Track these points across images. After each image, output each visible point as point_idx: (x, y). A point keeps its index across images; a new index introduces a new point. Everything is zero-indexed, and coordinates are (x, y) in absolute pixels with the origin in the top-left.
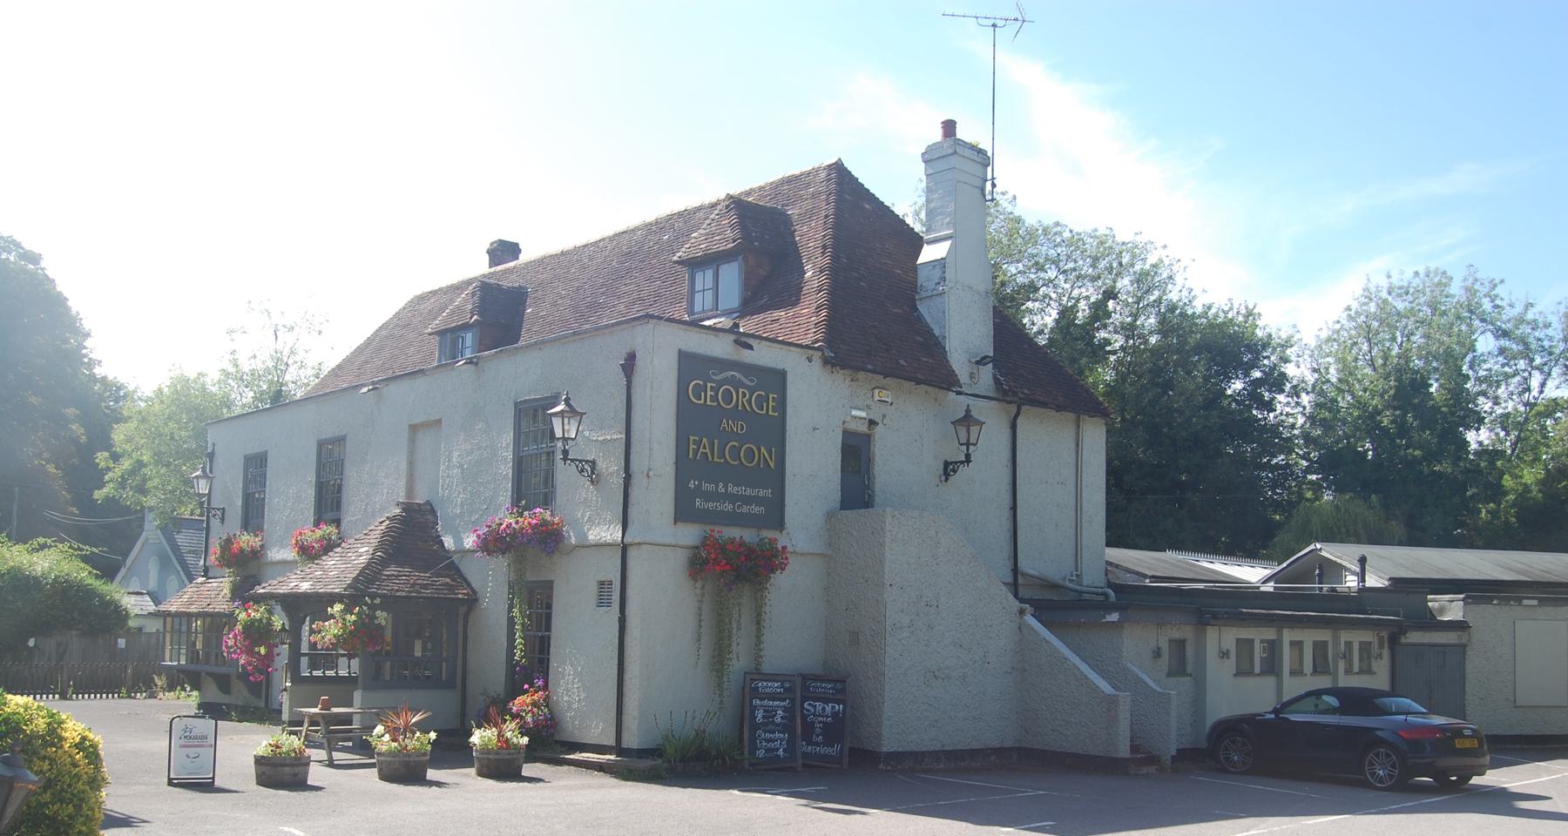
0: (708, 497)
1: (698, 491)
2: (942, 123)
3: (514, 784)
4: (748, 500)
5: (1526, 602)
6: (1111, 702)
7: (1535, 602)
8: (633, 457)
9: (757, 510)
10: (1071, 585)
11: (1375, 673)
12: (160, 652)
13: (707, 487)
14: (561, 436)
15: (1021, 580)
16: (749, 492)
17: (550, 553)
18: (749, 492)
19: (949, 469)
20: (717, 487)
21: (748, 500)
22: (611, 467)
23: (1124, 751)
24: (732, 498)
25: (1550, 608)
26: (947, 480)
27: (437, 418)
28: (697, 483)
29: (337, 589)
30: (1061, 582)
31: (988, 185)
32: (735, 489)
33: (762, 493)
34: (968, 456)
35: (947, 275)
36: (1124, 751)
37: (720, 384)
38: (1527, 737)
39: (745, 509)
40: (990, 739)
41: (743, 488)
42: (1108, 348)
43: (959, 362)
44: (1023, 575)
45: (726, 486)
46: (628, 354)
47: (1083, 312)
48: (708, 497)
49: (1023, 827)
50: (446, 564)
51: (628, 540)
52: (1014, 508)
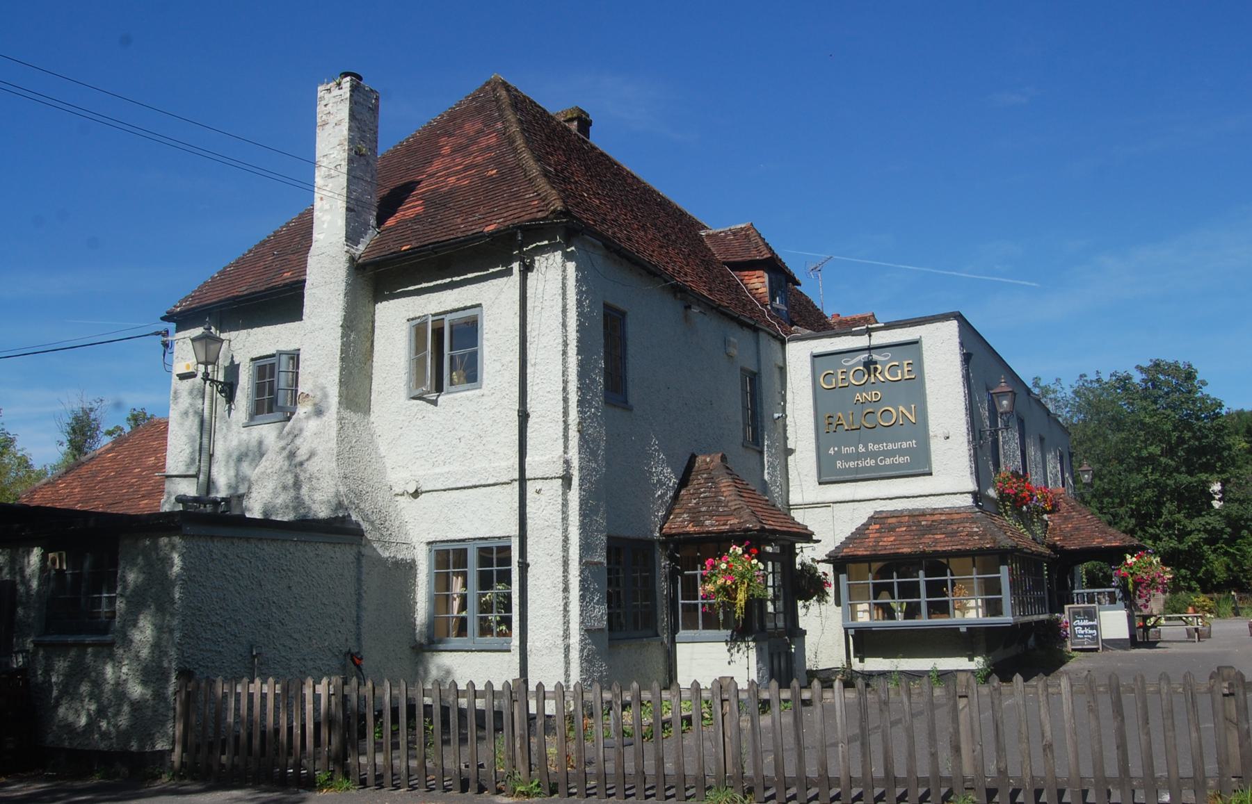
0: (848, 458)
1: (838, 455)
2: (302, 320)
4: (891, 454)
8: (847, 499)
12: (367, 392)
13: (844, 450)
14: (746, 694)
17: (469, 382)
18: (890, 446)
20: (857, 448)
21: (891, 454)
24: (874, 455)
27: (805, 676)
28: (836, 449)
31: (956, 516)
32: (876, 447)
33: (905, 445)
39: (888, 461)
41: (885, 444)
44: (189, 466)
45: (866, 446)
46: (349, 260)
48: (848, 458)
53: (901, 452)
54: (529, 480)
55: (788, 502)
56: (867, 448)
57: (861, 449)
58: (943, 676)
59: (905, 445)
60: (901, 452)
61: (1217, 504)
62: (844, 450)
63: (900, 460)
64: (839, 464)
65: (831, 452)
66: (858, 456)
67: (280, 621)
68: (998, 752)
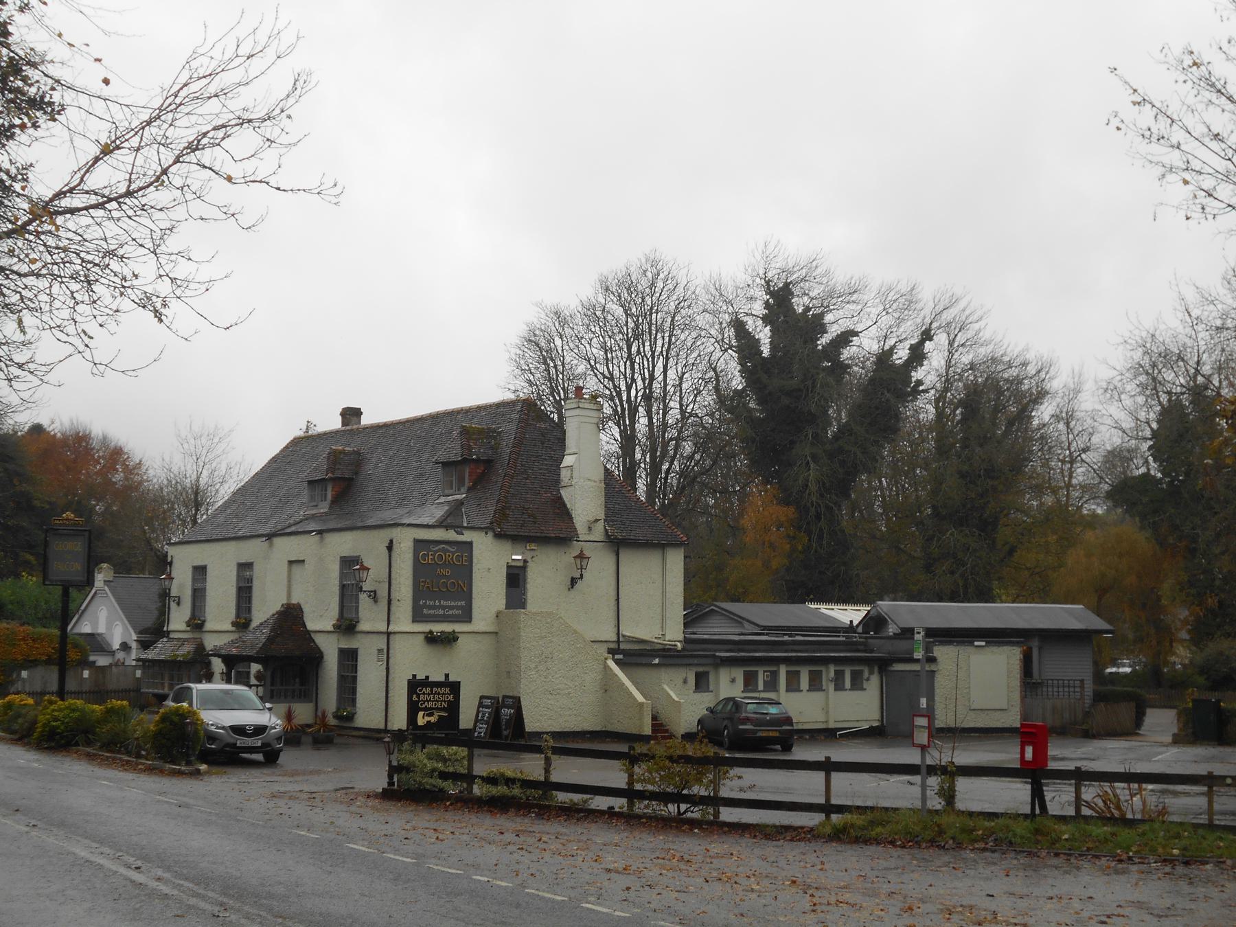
1: (425, 606)
3: (859, 692)
4: (452, 608)
5: (976, 643)
6: (641, 704)
7: (983, 644)
9: (456, 612)
10: (656, 641)
11: (865, 689)
13: (428, 603)
15: (621, 639)
16: (452, 603)
18: (452, 603)
19: (573, 582)
21: (452, 608)
22: (382, 593)
23: (647, 730)
24: (443, 608)
25: (995, 648)
26: (572, 587)
29: (253, 653)
30: (651, 640)
33: (460, 604)
34: (582, 575)
35: (574, 475)
36: (647, 730)
37: (437, 551)
38: (978, 728)
39: (450, 612)
40: (587, 725)
42: (921, 388)
43: (580, 520)
44: (624, 636)
45: (440, 602)
47: (902, 354)
48: (430, 608)
49: (1025, 780)
50: (307, 636)
51: (392, 628)
52: (618, 600)
53: (457, 608)
54: (289, 595)
55: (1026, 816)
56: (440, 602)
57: (437, 603)
58: (449, 868)
59: (460, 604)
60: (457, 608)
61: (682, 701)
62: (428, 603)
63: (456, 612)
64: (425, 611)
65: (421, 603)
66: (434, 607)
67: (391, 836)
68: (111, 152)
